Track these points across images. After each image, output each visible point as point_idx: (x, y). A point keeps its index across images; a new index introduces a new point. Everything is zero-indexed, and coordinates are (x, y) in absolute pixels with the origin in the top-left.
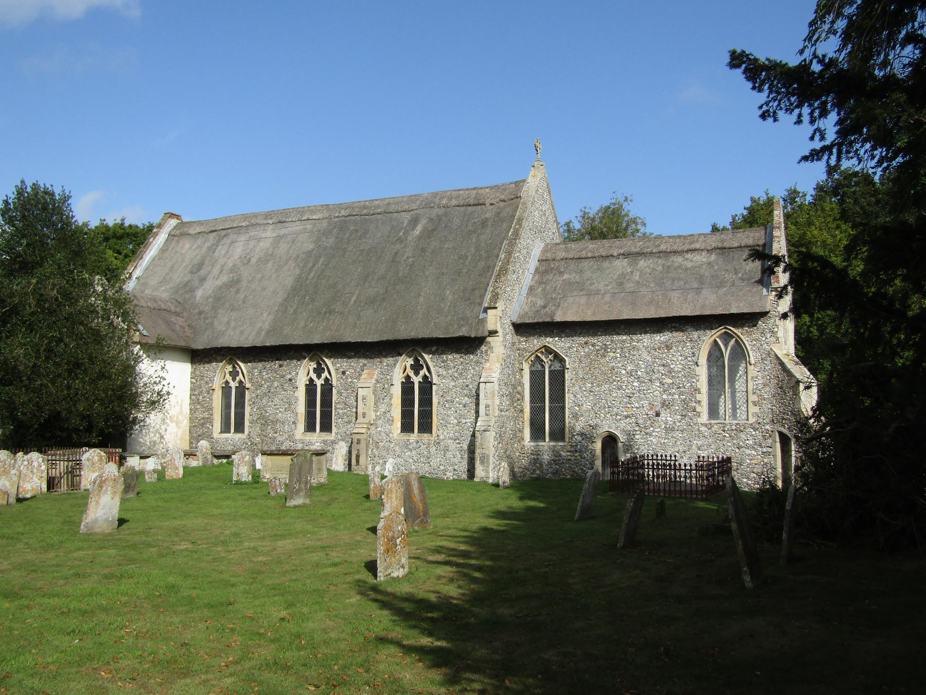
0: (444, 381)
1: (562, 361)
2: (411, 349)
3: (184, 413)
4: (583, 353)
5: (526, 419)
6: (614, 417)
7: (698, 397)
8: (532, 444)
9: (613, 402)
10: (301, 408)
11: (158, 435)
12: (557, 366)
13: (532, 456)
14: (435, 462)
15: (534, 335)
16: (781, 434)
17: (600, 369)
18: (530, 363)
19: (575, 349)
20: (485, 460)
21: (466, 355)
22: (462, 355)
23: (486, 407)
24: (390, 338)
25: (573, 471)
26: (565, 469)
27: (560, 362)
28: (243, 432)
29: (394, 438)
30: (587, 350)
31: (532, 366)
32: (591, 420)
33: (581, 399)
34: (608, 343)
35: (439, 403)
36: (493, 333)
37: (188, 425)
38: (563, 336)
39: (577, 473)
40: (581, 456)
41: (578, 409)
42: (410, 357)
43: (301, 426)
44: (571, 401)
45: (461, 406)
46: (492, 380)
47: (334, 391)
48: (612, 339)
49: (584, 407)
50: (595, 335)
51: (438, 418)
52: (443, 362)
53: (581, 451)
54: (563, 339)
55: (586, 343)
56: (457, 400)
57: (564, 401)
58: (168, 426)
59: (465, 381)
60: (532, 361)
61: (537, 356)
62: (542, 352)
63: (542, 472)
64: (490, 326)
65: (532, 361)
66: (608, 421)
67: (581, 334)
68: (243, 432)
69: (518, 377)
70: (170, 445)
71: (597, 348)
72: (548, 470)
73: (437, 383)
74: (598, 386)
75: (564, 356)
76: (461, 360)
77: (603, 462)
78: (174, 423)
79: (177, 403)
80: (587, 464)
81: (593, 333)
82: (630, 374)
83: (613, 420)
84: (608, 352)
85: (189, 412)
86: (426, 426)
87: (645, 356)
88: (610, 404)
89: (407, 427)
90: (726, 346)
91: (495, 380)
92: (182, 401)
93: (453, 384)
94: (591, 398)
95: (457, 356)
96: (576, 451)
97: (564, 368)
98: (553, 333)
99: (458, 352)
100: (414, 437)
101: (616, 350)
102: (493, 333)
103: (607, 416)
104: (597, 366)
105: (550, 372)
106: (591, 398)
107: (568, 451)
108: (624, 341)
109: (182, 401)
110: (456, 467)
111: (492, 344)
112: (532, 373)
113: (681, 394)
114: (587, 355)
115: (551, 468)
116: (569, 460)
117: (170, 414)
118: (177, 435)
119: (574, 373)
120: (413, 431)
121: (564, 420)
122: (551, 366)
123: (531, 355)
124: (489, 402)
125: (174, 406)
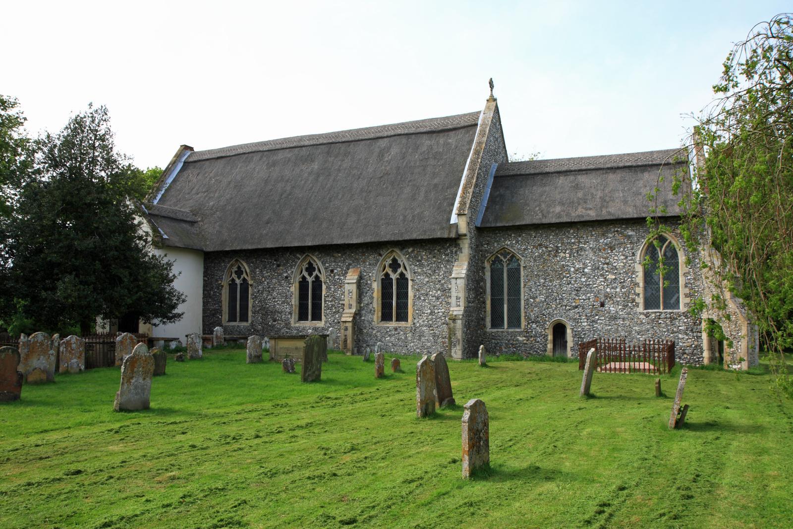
10: (295, 301)
47: (324, 287)
49: (537, 300)
60: (492, 261)
61: (497, 257)
74: (551, 281)
76: (434, 259)
84: (559, 253)
86: (402, 316)
100: (393, 324)
113: (623, 287)
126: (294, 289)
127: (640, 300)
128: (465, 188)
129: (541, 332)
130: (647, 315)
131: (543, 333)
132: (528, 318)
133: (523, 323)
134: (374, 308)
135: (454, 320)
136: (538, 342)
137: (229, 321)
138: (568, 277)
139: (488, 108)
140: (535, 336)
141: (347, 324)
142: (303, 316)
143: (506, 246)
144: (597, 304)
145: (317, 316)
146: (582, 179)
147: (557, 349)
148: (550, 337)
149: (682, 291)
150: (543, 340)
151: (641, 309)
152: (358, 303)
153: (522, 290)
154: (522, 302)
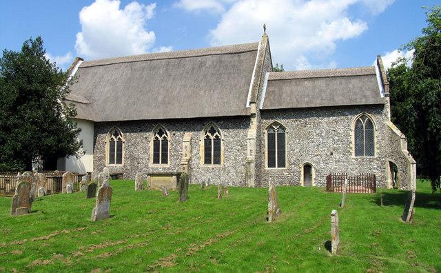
1: (284, 129)
7: (351, 146)
10: (151, 151)
12: (281, 131)
14: (223, 178)
16: (390, 162)
24: (200, 116)
28: (121, 163)
43: (152, 161)
47: (169, 143)
49: (295, 151)
68: (121, 163)
82: (318, 135)
86: (217, 161)
87: (325, 125)
89: (207, 161)
90: (364, 122)
100: (212, 166)
113: (343, 144)
120: (211, 163)
126: (151, 145)
127: (353, 151)
128: (254, 87)
130: (357, 160)
132: (289, 162)
133: (287, 164)
135: (249, 163)
137: (110, 163)
139: (263, 41)
141: (184, 166)
142: (156, 161)
144: (329, 153)
145: (165, 161)
146: (317, 83)
148: (302, 173)
149: (376, 146)
151: (353, 156)
152: (221, 18)
153: (286, 146)
154: (286, 153)
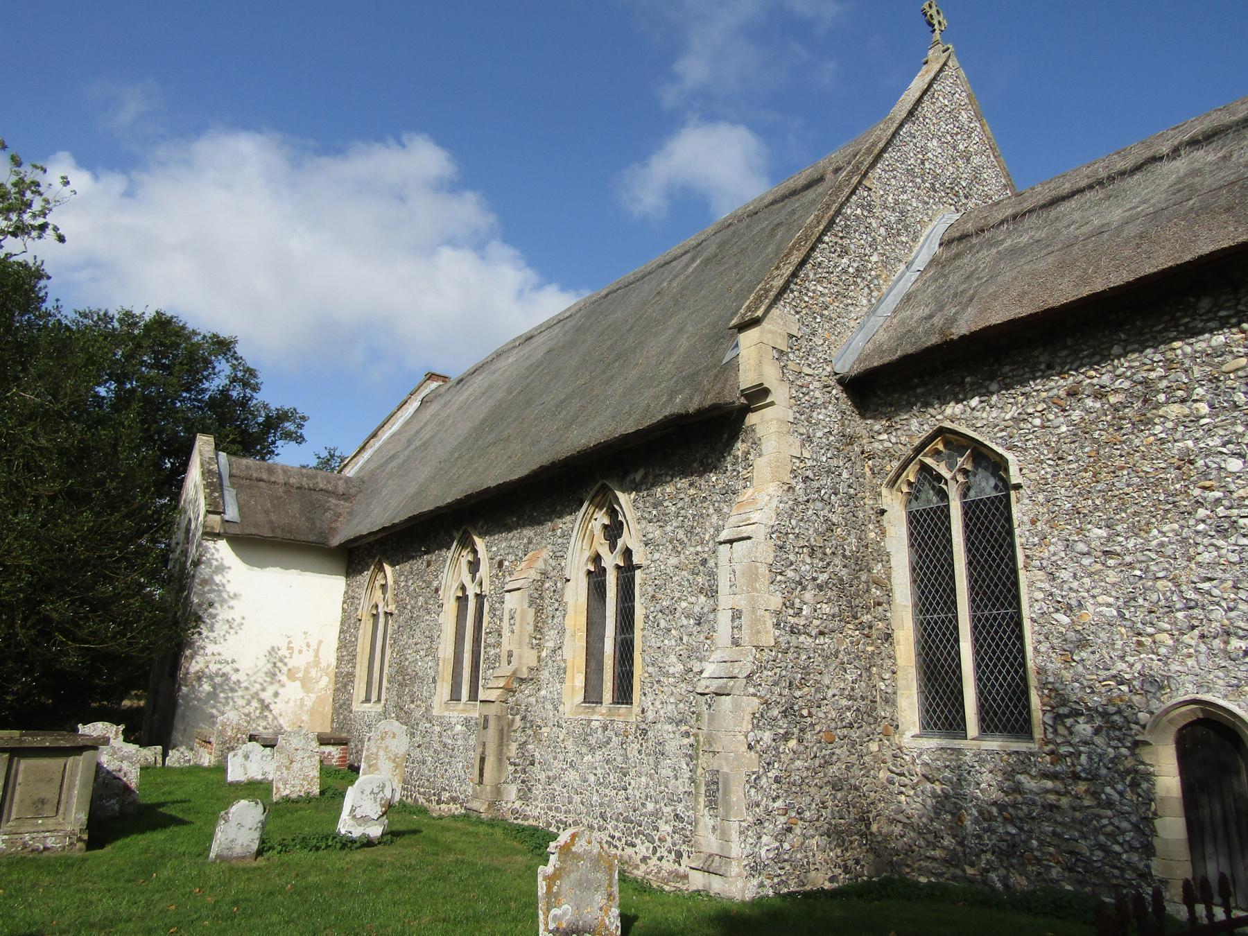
0: (657, 556)
1: (998, 466)
2: (596, 488)
3: (323, 664)
4: (1064, 428)
5: (901, 662)
6: (1217, 643)
8: (933, 743)
9: (1206, 586)
11: (255, 704)
12: (985, 487)
13: (929, 786)
15: (909, 406)
17: (1134, 469)
18: (905, 489)
19: (1037, 422)
20: (720, 795)
21: (701, 476)
22: (694, 478)
23: (733, 620)
25: (1072, 853)
26: (1041, 842)
27: (995, 474)
29: (567, 716)
30: (1076, 415)
31: (913, 496)
32: (1122, 658)
33: (1075, 585)
34: (1153, 375)
35: (647, 617)
36: (758, 395)
37: (332, 686)
38: (994, 387)
39: (1088, 862)
40: (1095, 795)
41: (1065, 620)
42: (601, 509)
43: (444, 690)
44: (1040, 595)
45: (692, 621)
46: (746, 531)
48: (1170, 355)
49: (1090, 613)
50: (1100, 356)
51: (644, 660)
52: (655, 506)
53: (1093, 777)
54: (994, 398)
55: (1072, 393)
56: (684, 604)
57: (1017, 597)
58: (283, 686)
59: (699, 548)
60: (910, 484)
61: (924, 468)
62: (937, 453)
63: (961, 843)
64: (747, 379)
65: (910, 484)
66: (1190, 662)
67: (1050, 367)
69: (872, 535)
70: (285, 723)
71: (1113, 399)
72: (979, 837)
73: (644, 563)
74: (1135, 531)
75: (1000, 450)
76: (692, 491)
77: (1194, 827)
78: (298, 683)
79: (308, 645)
80: (1123, 832)
81: (1092, 355)
83: (1212, 653)
84: (1158, 406)
85: (334, 663)
86: (624, 693)
88: (1191, 595)
89: (592, 695)
91: (759, 533)
92: (320, 642)
93: (673, 561)
94: (1112, 577)
95: (682, 483)
96: (1076, 777)
97: (1005, 486)
98: (964, 390)
99: (684, 473)
101: (1189, 389)
102: (758, 395)
103: (1186, 639)
104: (1119, 462)
105: (969, 510)
106: (1112, 577)
107: (1045, 775)
108: (1219, 352)
109: (320, 642)
110: (680, 808)
111: (760, 431)
112: (914, 519)
114: (1081, 432)
115: (994, 832)
116: (1052, 807)
117: (290, 666)
118: (302, 704)
119: (1041, 498)
121: (1023, 665)
122: (969, 489)
123: (904, 467)
124: (741, 602)
125: (300, 652)
129: (1116, 759)
131: (1129, 763)
134: (564, 661)
136: (1110, 804)
138: (1218, 501)
140: (1093, 777)
143: (947, 424)
147: (1209, 849)
150: (1128, 794)
